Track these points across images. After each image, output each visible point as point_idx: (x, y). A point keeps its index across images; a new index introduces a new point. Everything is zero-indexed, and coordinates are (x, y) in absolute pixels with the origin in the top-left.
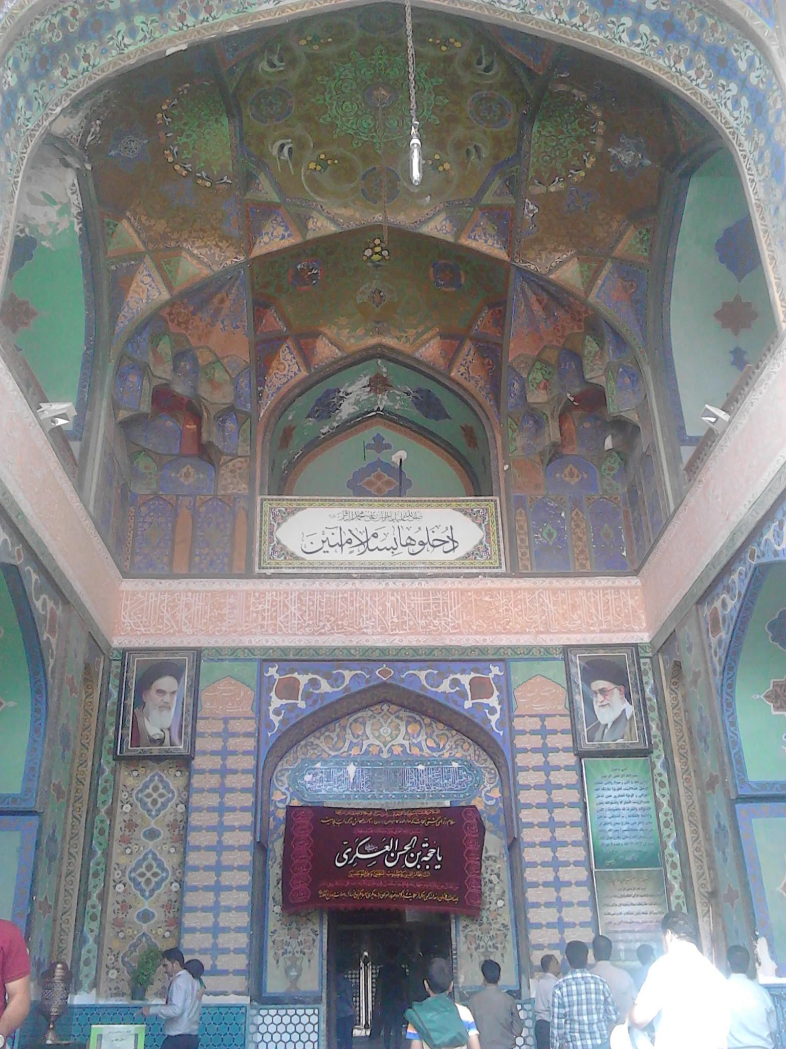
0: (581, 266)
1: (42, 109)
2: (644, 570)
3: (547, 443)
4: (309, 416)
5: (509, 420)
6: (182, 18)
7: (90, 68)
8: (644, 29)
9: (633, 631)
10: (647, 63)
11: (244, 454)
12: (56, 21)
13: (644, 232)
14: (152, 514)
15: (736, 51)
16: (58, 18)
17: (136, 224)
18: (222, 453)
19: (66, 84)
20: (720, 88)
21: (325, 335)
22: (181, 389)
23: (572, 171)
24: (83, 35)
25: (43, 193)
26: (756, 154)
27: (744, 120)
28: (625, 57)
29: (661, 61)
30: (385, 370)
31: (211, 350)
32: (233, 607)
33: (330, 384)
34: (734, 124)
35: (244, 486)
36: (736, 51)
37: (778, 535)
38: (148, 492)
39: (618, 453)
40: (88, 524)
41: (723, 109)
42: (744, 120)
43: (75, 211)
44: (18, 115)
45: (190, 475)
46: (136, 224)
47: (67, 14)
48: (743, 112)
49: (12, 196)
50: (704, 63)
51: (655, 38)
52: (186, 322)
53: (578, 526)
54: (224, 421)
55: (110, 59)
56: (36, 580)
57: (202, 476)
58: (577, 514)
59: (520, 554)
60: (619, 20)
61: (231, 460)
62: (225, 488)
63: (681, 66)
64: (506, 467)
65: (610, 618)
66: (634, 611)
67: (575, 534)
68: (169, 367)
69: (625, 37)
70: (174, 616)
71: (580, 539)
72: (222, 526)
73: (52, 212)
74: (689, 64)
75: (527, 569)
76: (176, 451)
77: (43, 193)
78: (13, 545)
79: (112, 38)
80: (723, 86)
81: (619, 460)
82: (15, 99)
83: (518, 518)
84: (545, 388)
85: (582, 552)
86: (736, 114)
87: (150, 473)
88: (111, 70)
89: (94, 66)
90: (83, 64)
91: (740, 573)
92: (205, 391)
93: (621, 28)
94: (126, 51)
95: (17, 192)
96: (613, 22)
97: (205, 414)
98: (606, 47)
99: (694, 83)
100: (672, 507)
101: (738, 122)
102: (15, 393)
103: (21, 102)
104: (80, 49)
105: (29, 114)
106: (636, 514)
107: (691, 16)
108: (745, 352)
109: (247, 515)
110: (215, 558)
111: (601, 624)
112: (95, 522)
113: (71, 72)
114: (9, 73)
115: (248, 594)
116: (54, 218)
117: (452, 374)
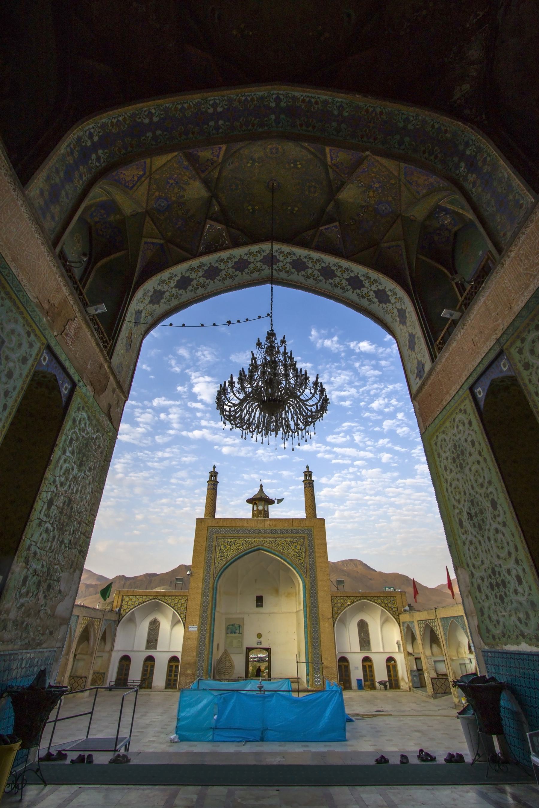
47: (426, 155)
51: (140, 120)
60: (160, 117)
90: (437, 126)
96: (162, 115)
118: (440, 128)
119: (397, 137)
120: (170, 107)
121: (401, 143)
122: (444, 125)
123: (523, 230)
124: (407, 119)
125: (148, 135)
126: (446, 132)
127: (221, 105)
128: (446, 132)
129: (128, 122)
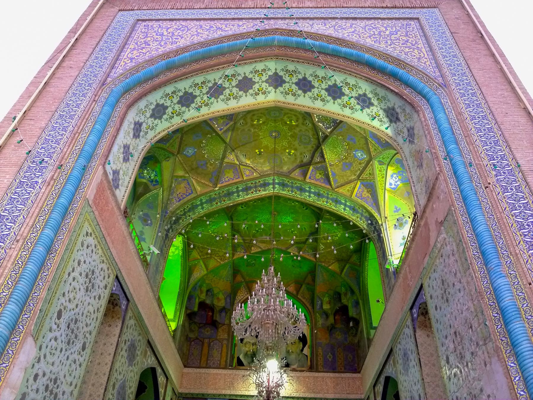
6: (217, 203)
9: (358, 394)
18: (219, 323)
22: (208, 302)
24: (189, 211)
32: (220, 379)
40: (176, 351)
43: (180, 248)
45: (208, 331)
54: (221, 312)
64: (316, 331)
65: (350, 389)
66: (359, 387)
68: (204, 294)
70: (200, 382)
71: (340, 359)
76: (204, 322)
84: (329, 303)
85: (341, 364)
92: (215, 302)
103: (171, 231)
111: (347, 391)
113: (185, 220)
115: (225, 375)
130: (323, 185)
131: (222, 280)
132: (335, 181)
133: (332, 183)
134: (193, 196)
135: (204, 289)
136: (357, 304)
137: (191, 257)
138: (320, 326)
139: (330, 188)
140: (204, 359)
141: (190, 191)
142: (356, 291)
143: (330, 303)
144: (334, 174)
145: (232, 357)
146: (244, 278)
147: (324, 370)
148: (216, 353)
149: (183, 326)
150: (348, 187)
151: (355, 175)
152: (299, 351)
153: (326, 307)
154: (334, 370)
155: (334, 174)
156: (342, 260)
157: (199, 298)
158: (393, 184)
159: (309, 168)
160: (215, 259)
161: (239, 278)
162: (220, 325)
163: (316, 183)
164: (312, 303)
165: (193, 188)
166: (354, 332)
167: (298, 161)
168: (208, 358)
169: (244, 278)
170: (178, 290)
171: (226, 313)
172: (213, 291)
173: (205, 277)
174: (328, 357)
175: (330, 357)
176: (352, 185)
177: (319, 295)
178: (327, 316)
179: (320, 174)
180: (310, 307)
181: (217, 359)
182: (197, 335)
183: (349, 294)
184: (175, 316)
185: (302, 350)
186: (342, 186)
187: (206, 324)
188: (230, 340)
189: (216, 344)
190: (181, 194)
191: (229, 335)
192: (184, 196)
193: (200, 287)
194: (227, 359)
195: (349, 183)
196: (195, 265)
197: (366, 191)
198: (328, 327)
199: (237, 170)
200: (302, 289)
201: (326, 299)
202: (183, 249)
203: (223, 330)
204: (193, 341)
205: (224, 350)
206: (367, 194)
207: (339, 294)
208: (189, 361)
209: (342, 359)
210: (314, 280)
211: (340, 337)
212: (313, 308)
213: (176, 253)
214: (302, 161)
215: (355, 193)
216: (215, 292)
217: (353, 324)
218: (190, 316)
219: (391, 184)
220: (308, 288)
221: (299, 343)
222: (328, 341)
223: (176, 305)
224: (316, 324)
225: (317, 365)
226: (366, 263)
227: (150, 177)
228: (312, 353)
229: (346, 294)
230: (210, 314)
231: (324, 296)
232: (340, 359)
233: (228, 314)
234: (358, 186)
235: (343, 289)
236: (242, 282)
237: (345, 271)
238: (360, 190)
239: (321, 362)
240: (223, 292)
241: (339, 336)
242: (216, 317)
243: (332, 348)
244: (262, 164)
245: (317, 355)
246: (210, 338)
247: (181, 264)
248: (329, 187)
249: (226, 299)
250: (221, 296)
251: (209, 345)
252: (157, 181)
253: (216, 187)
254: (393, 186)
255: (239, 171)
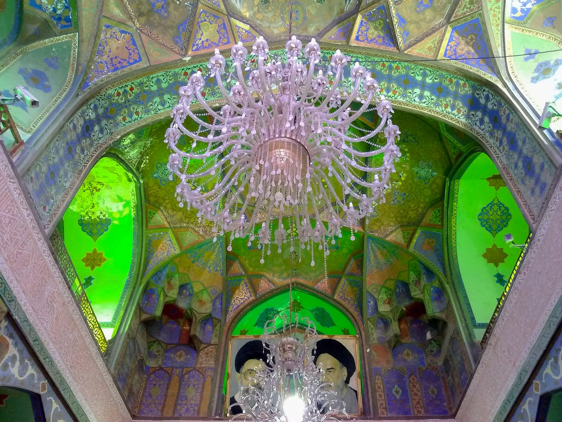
0: (404, 233)
1: (109, 135)
2: (458, 414)
3: (392, 335)
4: (255, 326)
5: (369, 322)
7: (139, 119)
8: (427, 93)
10: (430, 111)
11: (215, 343)
12: (121, 91)
13: (437, 212)
14: (156, 379)
15: (478, 94)
16: (123, 90)
17: (165, 214)
18: (201, 343)
19: (124, 125)
20: (472, 116)
21: (265, 277)
22: (182, 304)
23: (395, 182)
25: (117, 196)
26: (498, 144)
27: (488, 129)
28: (418, 110)
29: (437, 109)
30: (298, 297)
31: (201, 283)
33: (268, 304)
34: (482, 133)
35: (212, 362)
36: (478, 94)
37: (555, 367)
38: (157, 366)
39: (435, 341)
40: (109, 379)
41: (475, 127)
42: (488, 129)
43: (132, 204)
44: (93, 134)
45: (181, 357)
46: (165, 214)
47: (128, 89)
48: (486, 125)
49: (81, 171)
50: (461, 105)
51: (433, 97)
52: (189, 267)
53: (414, 386)
54: (205, 324)
55: (150, 115)
56: (57, 408)
57: (189, 356)
58: (413, 379)
59: (379, 405)
60: (413, 91)
61: (206, 347)
62: (201, 363)
63: (449, 109)
64: (368, 350)
67: (413, 391)
69: (417, 99)
71: (416, 394)
72: (197, 387)
73: (120, 206)
74: (453, 108)
75: (384, 414)
77: (117, 196)
78: (39, 379)
79: (152, 105)
80: (473, 115)
81: (436, 345)
82: (93, 126)
83: (377, 381)
84: (389, 303)
85: (418, 403)
86: (482, 127)
87: (159, 355)
88: (150, 121)
89: (141, 118)
90: (135, 116)
91: (530, 403)
92: (195, 306)
93: (415, 95)
94: (159, 112)
95: (85, 171)
96: (410, 93)
97: (194, 319)
98: (407, 105)
99: (457, 117)
100: (474, 367)
101: (484, 131)
102: (60, 279)
104: (134, 108)
105: (100, 136)
106: (450, 377)
107: (451, 81)
108: (503, 276)
109: (212, 380)
110: (190, 407)
112: (114, 377)
113: (128, 119)
114: (90, 111)
116: (121, 208)
117: (335, 297)
118: (131, 117)
119: (164, 85)
120: (400, 97)
121: (158, 82)
122: (129, 122)
123: (31, 217)
124: (163, 105)
125: (431, 81)
126: (124, 119)
127: (350, 83)
128: (124, 119)
129: (444, 102)
130: (382, 48)
131: (207, 269)
132: (406, 34)
133: (400, 40)
134: (143, 64)
135: (176, 282)
136: (440, 293)
137: (152, 223)
138: (376, 341)
139: (395, 50)
140: (170, 402)
141: (136, 57)
142: (436, 269)
143: (389, 302)
144: (402, 20)
145: (222, 399)
146: (245, 269)
147: (390, 415)
148: (191, 393)
149: (131, 338)
150: (429, 42)
151: (442, 15)
152: (341, 383)
153: (383, 308)
154: (406, 413)
155: (402, 20)
156: (409, 224)
157: (166, 296)
158: (519, 9)
159: (355, 20)
160: (195, 231)
161: (236, 268)
162: (203, 346)
163: (368, 46)
164: (360, 306)
165: (141, 51)
166: (435, 349)
167: (335, 12)
168: (177, 401)
169: (245, 269)
170: (126, 277)
171: (214, 327)
172: (192, 288)
173: (177, 261)
174: (394, 392)
175: (397, 392)
176: (436, 36)
177: (370, 290)
178: (386, 324)
179: (376, 28)
180: (356, 314)
181: (193, 402)
182: (160, 363)
183: (424, 280)
184: (115, 318)
185: (347, 381)
186: (417, 41)
187: (179, 344)
188: (219, 370)
189: (193, 377)
190: (119, 59)
191: (217, 361)
192: (125, 64)
193: (170, 277)
194: (211, 402)
195: (430, 34)
196: (160, 238)
197: (463, 42)
198: (389, 342)
199: (225, 28)
200: (341, 285)
201: (383, 297)
202: (136, 206)
203: (207, 354)
204: (154, 372)
205: (208, 386)
206: (466, 49)
207: (406, 285)
208: (143, 407)
209: (419, 394)
210: (360, 264)
211: (411, 358)
212: (362, 314)
213: (124, 214)
214: (342, 11)
215: (442, 51)
216: (196, 290)
217: (432, 335)
218: (149, 325)
219: (514, 10)
220: (350, 283)
221: (341, 368)
222: (392, 366)
223: (121, 301)
224: (367, 338)
225: (375, 407)
226: (453, 220)
227: (55, 10)
228: (365, 387)
229: (418, 283)
230: (187, 328)
231: (379, 293)
232: (416, 394)
233: (217, 327)
234: (448, 35)
235: (413, 276)
236: (242, 275)
237: (414, 240)
238: (452, 44)
239: (381, 401)
240: (209, 290)
241: (410, 358)
242: (195, 329)
243: (400, 377)
244: (271, 23)
245: (374, 391)
246: (182, 368)
247: (134, 233)
248: (392, 49)
249: (214, 302)
250: (205, 297)
251: (181, 378)
252: (68, 20)
253: (185, 56)
254: (519, 14)
255: (228, 28)
